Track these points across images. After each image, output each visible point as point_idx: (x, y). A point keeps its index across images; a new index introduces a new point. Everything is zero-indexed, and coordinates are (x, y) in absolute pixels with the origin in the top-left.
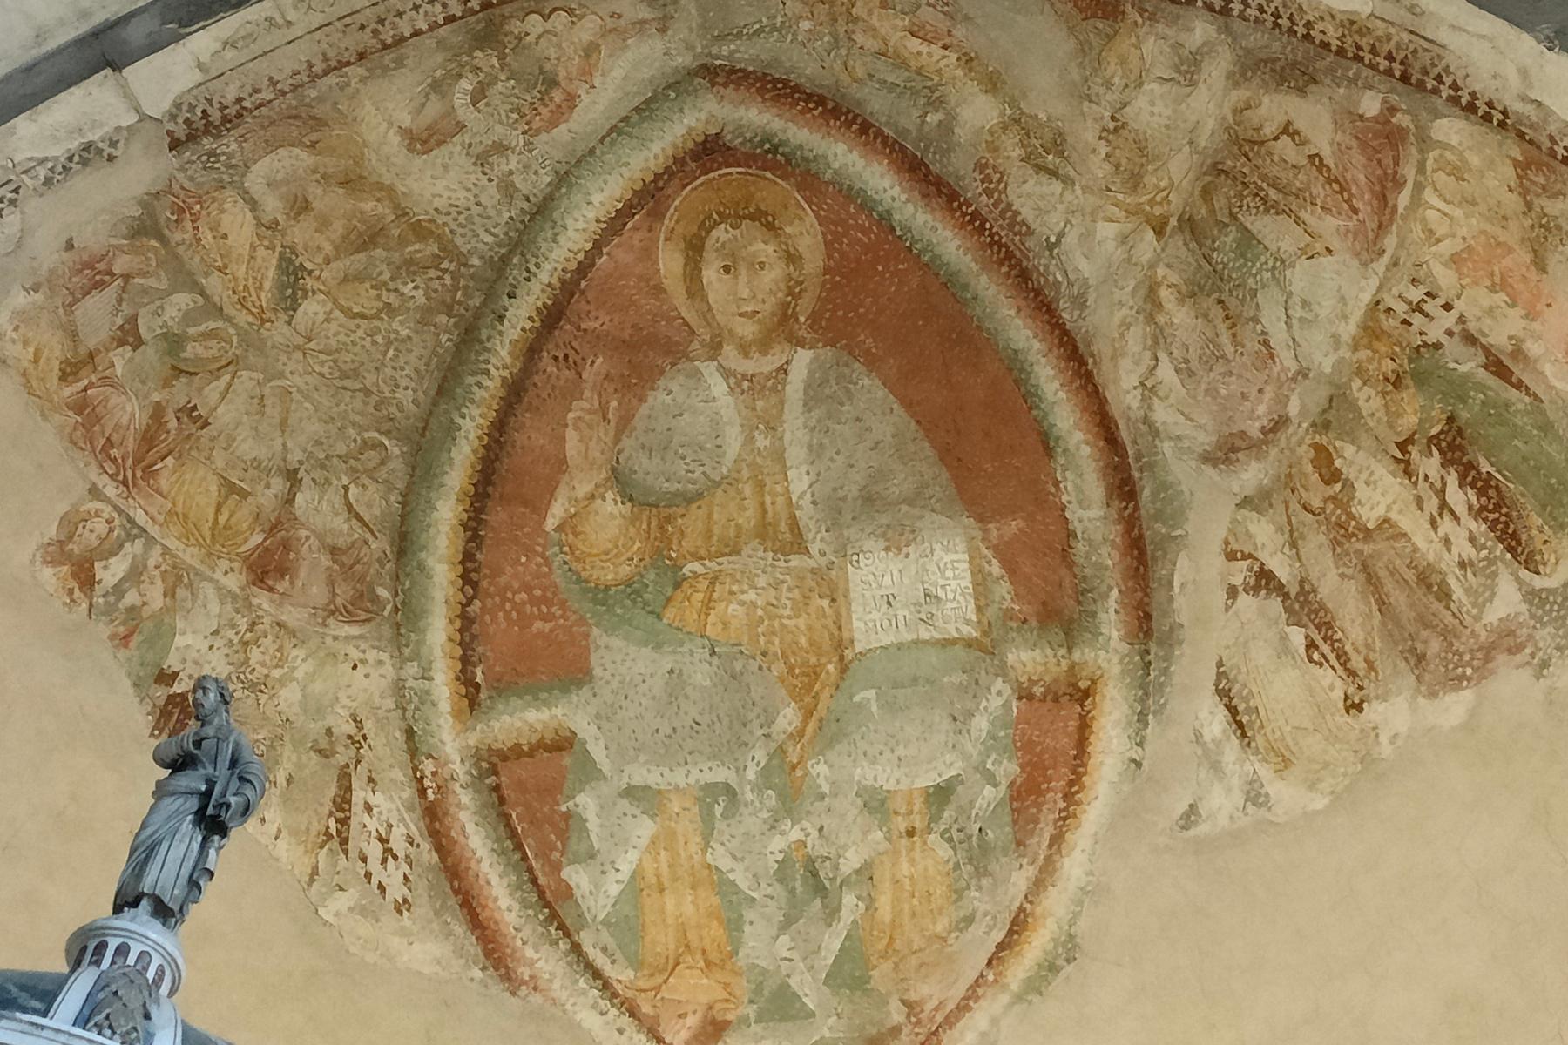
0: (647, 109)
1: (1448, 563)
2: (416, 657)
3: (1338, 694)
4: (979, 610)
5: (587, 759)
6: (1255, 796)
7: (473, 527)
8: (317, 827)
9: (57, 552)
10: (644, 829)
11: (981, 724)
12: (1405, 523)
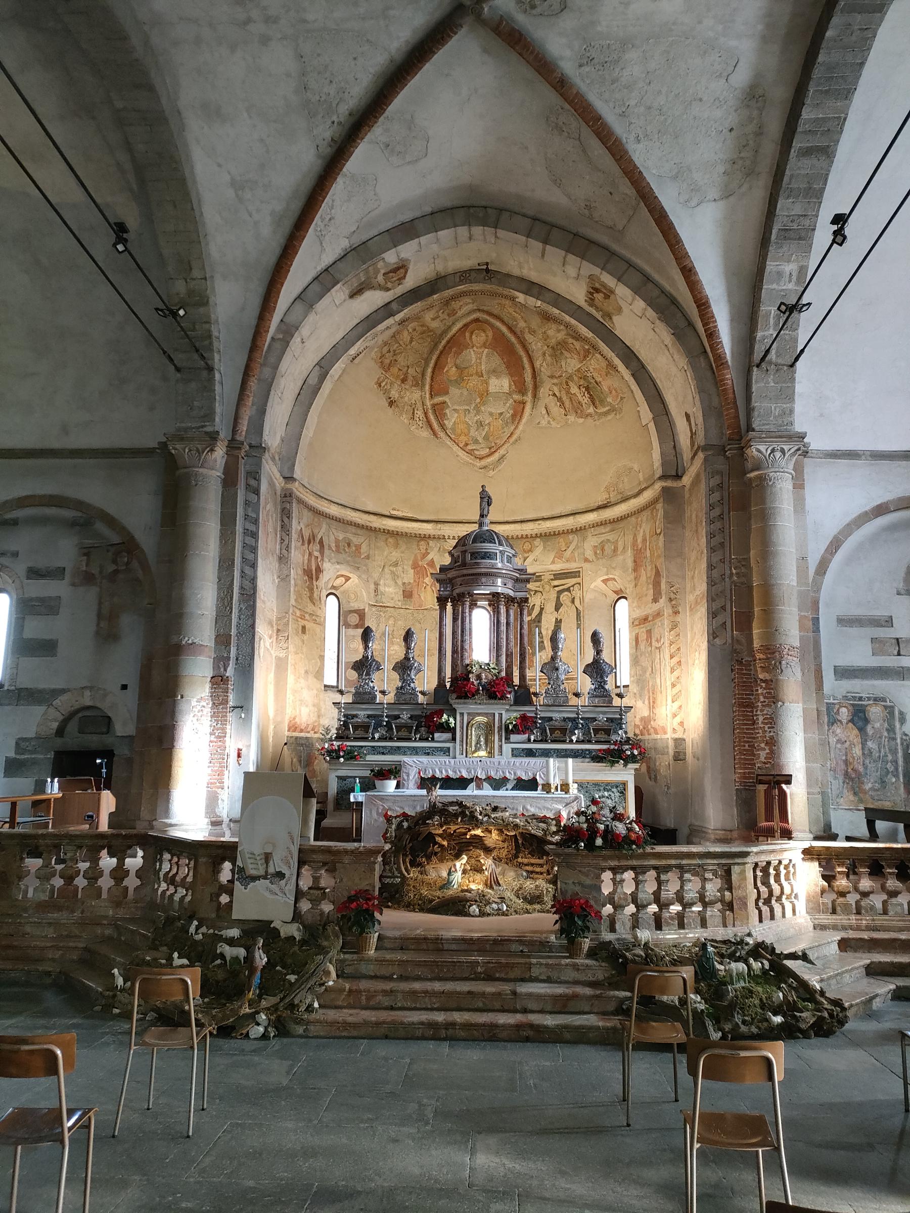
0: (469, 313)
1: (583, 402)
6: (549, 422)
7: (433, 372)
10: (456, 415)
11: (508, 405)
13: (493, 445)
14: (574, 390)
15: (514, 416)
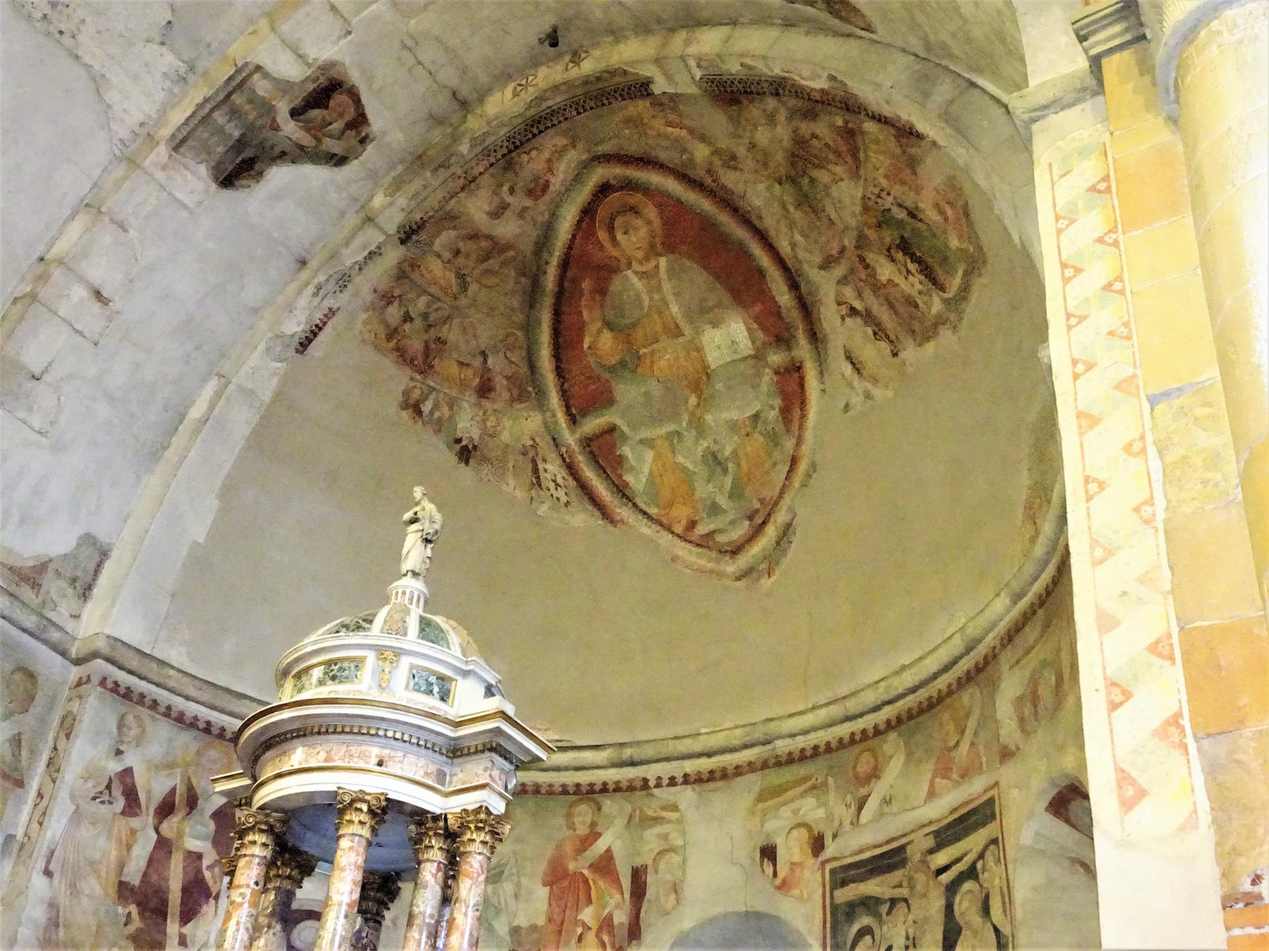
0: (578, 179)
1: (914, 293)
2: (548, 410)
3: (889, 351)
4: (753, 342)
5: (623, 433)
6: (868, 396)
7: (557, 356)
8: (528, 482)
9: (405, 405)
10: (649, 455)
12: (897, 281)
13: (757, 506)
14: (885, 271)
15: (785, 412)
